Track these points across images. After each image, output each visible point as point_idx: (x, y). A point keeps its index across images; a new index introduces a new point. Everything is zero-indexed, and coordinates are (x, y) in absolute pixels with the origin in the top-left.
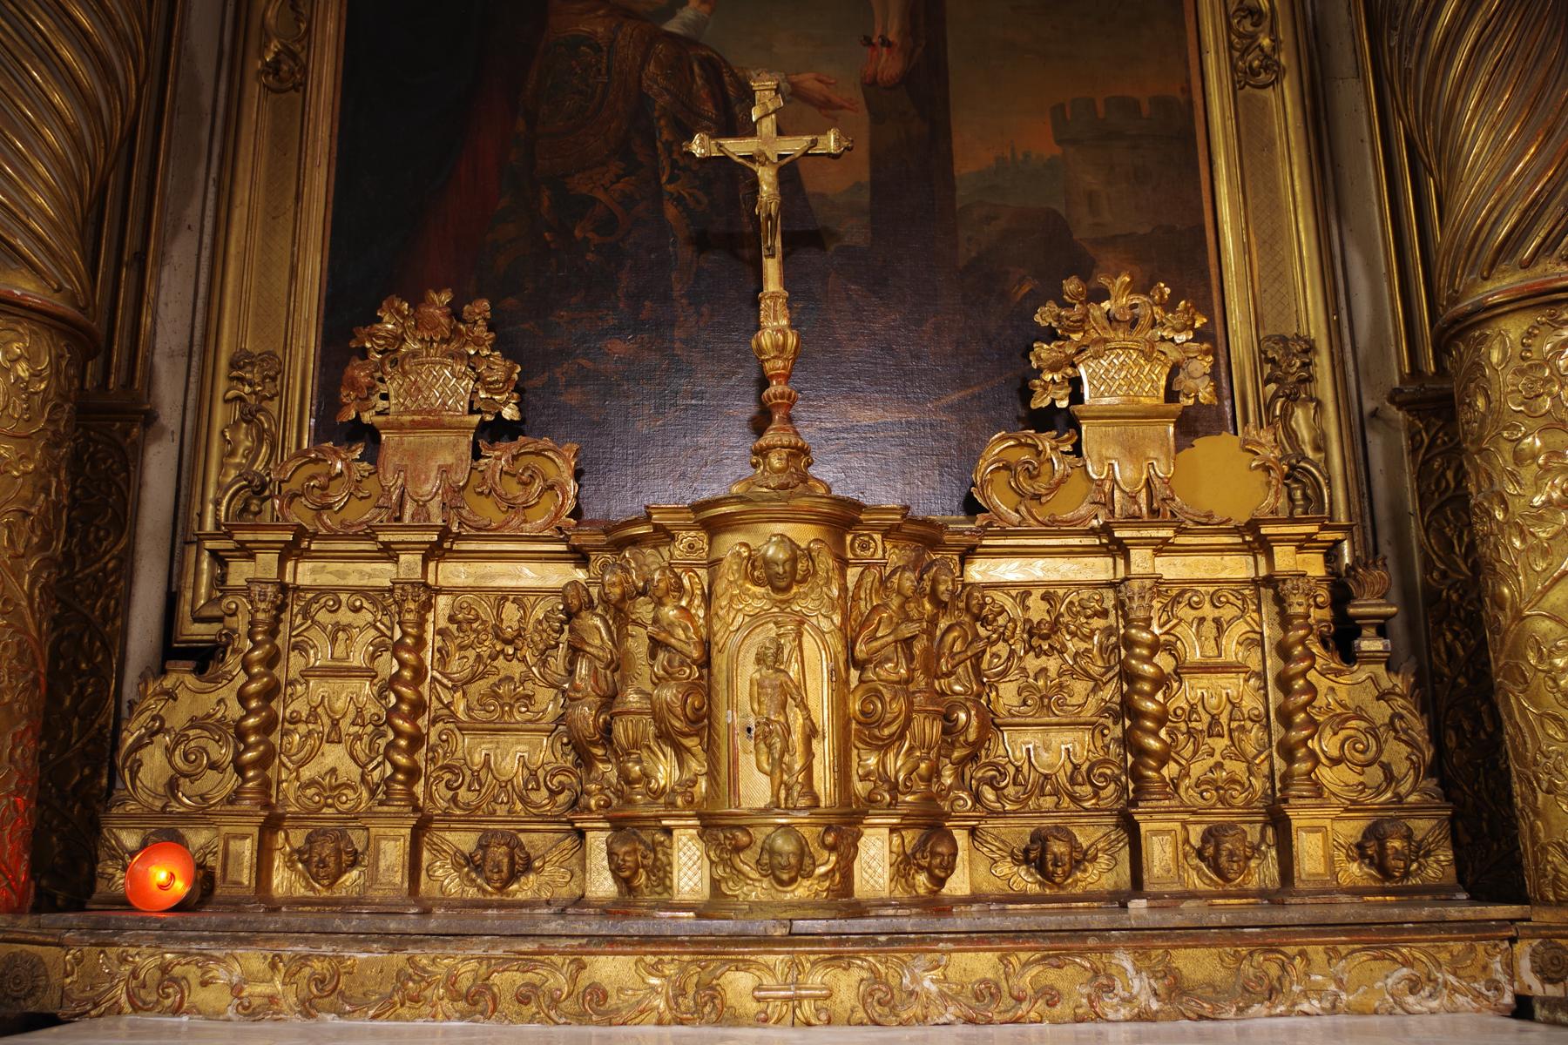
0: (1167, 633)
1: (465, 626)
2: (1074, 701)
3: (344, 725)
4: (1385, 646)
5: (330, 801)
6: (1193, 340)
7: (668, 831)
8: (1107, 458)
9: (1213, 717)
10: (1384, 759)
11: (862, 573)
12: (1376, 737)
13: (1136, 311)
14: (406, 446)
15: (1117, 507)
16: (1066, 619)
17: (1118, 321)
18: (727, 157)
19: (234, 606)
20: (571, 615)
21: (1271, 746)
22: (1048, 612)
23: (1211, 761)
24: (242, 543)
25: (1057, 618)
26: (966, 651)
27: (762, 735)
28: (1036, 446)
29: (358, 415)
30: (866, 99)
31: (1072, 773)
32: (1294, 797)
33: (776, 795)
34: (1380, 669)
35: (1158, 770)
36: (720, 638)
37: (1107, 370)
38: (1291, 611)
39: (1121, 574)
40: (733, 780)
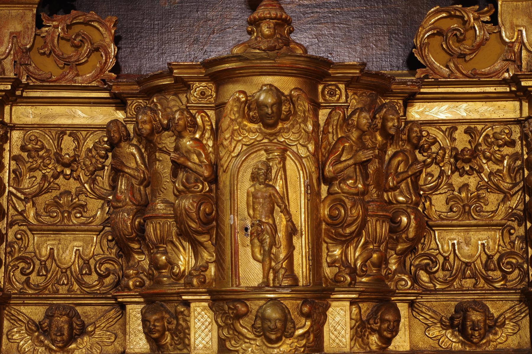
1: (33, 153)
2: (488, 208)
7: (187, 304)
15: (524, 63)
16: (484, 147)
20: (113, 145)
25: (476, 147)
28: (462, 17)
31: (487, 262)
33: (266, 276)
36: (225, 161)
40: (235, 266)
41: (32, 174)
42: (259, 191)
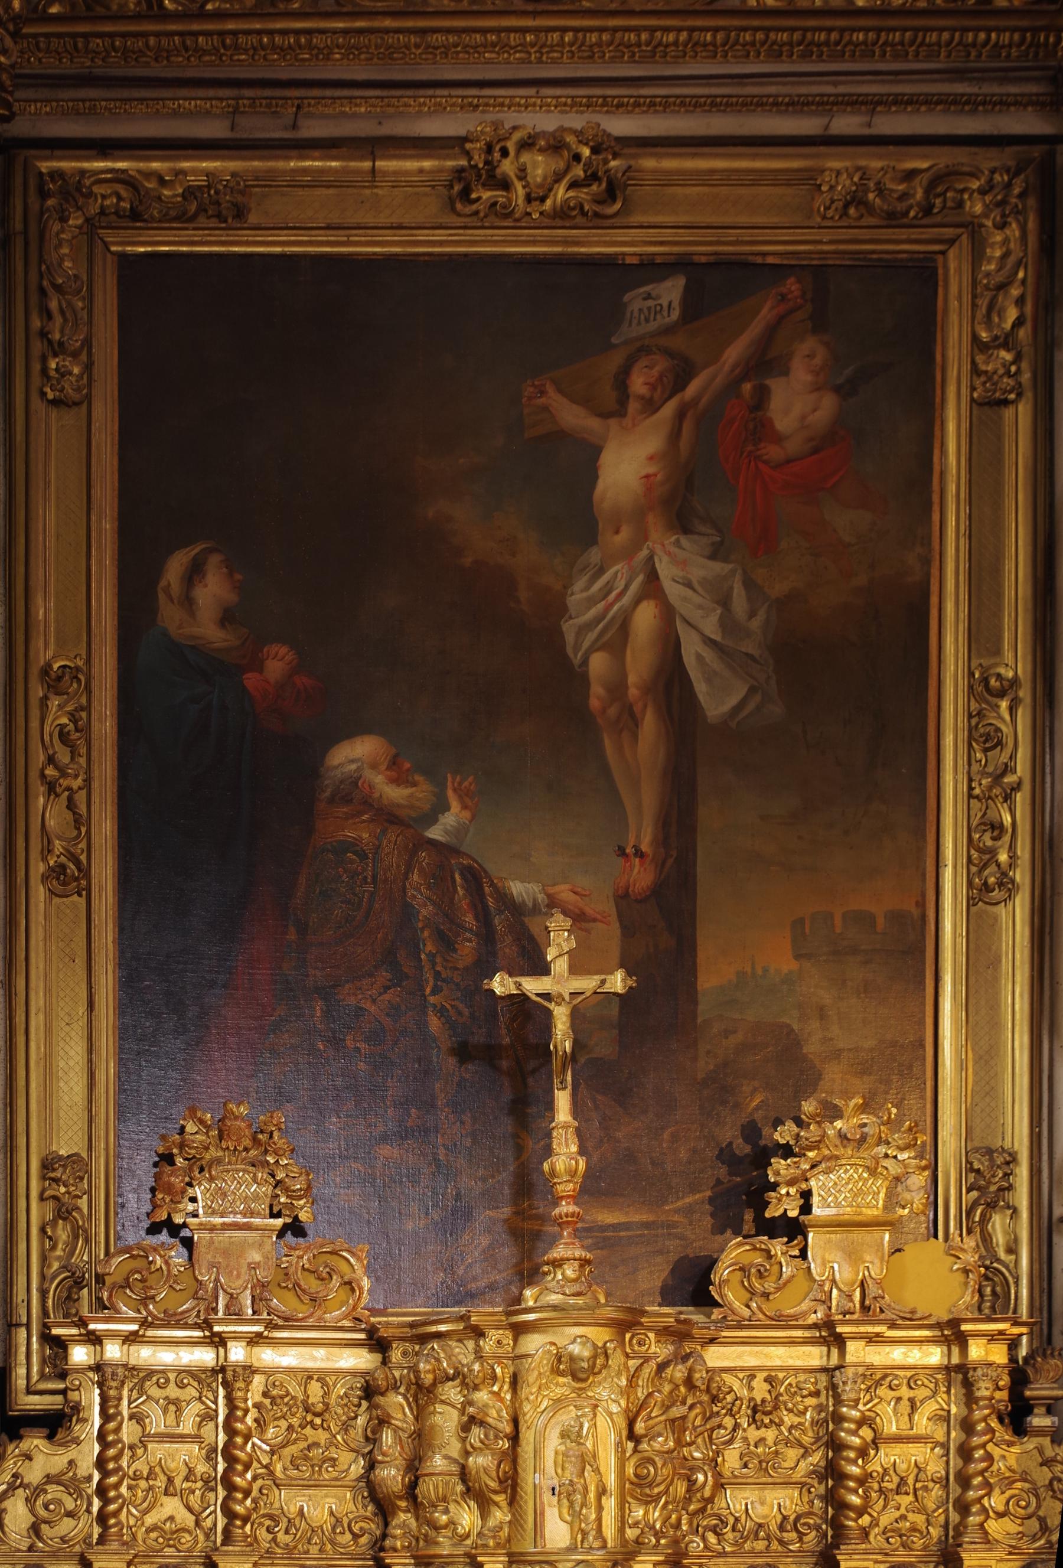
0: (869, 1410)
1: (279, 1401)
2: (786, 1465)
3: (178, 1481)
4: (1053, 1423)
5: (171, 1542)
6: (915, 1158)
8: (829, 1262)
9: (902, 1479)
10: (1041, 1513)
11: (642, 1365)
12: (1037, 1496)
13: (866, 1130)
14: (216, 1244)
15: (834, 1303)
16: (785, 1398)
17: (848, 1140)
18: (524, 994)
19: (77, 1383)
21: (947, 1502)
22: (769, 1391)
23: (897, 1514)
24: (93, 1332)
25: (776, 1398)
26: (705, 1424)
27: (565, 1493)
28: (768, 1251)
29: (169, 1215)
30: (618, 911)
31: (782, 1522)
32: (968, 1543)
33: (574, 1538)
34: (1046, 1441)
35: (856, 1521)
37: (835, 1183)
38: (978, 1394)
39: (834, 1361)
41: (276, 1423)
42: (571, 1449)
